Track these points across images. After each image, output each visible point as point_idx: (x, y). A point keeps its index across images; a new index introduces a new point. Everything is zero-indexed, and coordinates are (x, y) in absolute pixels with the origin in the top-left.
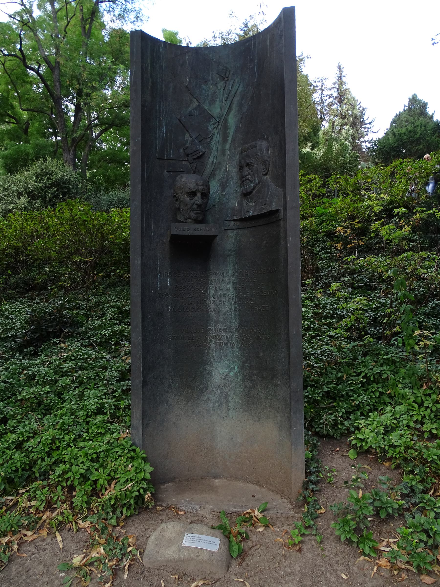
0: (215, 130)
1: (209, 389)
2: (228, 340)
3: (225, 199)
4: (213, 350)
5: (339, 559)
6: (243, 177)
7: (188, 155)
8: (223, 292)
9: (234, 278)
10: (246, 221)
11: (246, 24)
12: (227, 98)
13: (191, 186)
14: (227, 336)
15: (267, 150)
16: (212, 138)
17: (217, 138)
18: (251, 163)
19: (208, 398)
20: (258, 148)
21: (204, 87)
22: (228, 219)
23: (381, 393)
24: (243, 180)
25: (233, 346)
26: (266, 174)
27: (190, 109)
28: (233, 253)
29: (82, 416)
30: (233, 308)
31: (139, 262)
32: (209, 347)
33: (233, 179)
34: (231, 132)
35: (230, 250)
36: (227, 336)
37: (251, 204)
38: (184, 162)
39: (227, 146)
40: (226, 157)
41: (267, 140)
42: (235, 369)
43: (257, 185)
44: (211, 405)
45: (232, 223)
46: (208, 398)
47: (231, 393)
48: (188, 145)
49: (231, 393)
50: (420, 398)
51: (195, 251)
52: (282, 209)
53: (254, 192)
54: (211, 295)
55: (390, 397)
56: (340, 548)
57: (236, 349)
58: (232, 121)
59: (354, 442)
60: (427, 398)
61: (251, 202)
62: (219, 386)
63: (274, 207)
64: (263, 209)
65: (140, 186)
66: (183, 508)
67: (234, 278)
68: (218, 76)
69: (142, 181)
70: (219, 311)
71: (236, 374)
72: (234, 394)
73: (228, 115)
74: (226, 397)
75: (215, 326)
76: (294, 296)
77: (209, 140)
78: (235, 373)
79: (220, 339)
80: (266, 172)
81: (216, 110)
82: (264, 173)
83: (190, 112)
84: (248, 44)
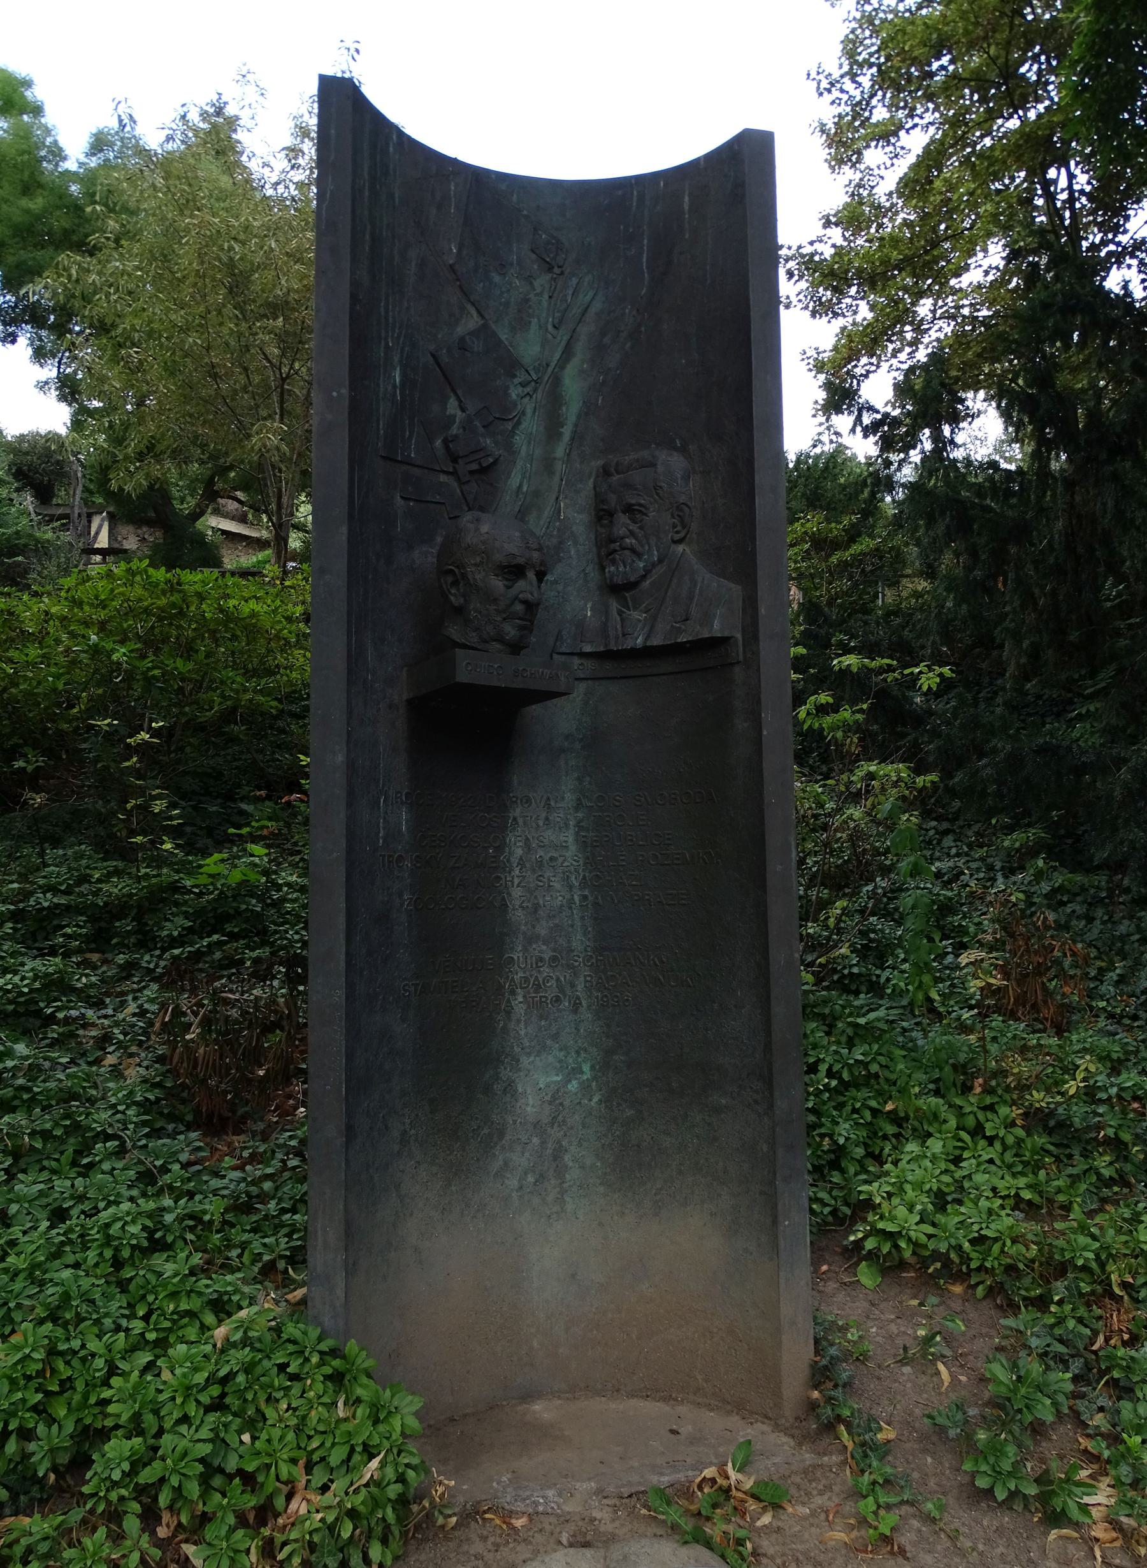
0: (526, 400)
1: (507, 1137)
2: (562, 991)
3: (553, 594)
4: (519, 1021)
5: (1001, 1550)
6: (614, 541)
7: (455, 460)
8: (546, 854)
9: (580, 815)
10: (618, 660)
11: (221, 109)
12: (561, 322)
13: (511, 548)
14: (558, 980)
15: (686, 478)
16: (519, 423)
17: (531, 424)
18: (641, 505)
19: (506, 1164)
20: (660, 468)
21: (497, 279)
22: (563, 650)
23: (875, 1112)
24: (607, 549)
25: (576, 1007)
26: (680, 541)
27: (460, 330)
28: (578, 746)
29: (97, 1265)
30: (576, 898)
31: (340, 758)
32: (508, 1013)
33: (576, 543)
34: (571, 412)
35: (567, 737)
36: (558, 980)
37: (636, 615)
38: (443, 478)
39: (560, 451)
40: (556, 479)
41: (683, 450)
42: (582, 1073)
43: (654, 565)
44: (513, 1183)
45: (576, 661)
46: (506, 1164)
47: (570, 1143)
48: (455, 430)
49: (570, 1143)
50: (971, 1117)
51: (467, 733)
52: (739, 636)
53: (646, 584)
54: (514, 861)
55: (896, 1119)
56: (989, 1521)
57: (586, 1015)
58: (573, 386)
59: (870, 1244)
60: (989, 1115)
61: (635, 609)
62: (536, 1125)
63: (717, 628)
64: (679, 631)
65: (344, 529)
66: (520, 1506)
67: (580, 815)
68: (534, 256)
69: (351, 516)
70: (536, 908)
71: (585, 1087)
72: (580, 1145)
73: (563, 368)
74: (558, 1153)
75: (525, 949)
76: (779, 868)
77: (509, 426)
78: (581, 1083)
79: (538, 987)
80: (682, 535)
81: (529, 347)
82: (677, 537)
83: (462, 339)
84: (620, 193)
